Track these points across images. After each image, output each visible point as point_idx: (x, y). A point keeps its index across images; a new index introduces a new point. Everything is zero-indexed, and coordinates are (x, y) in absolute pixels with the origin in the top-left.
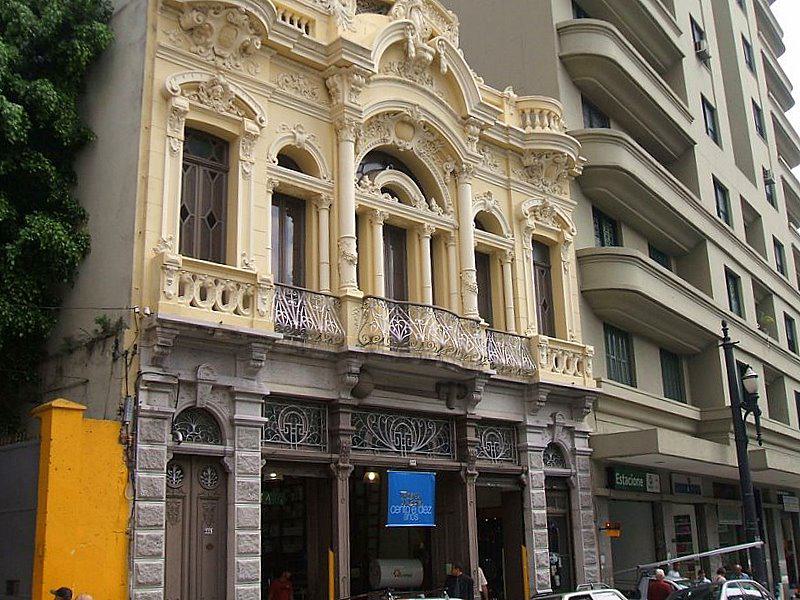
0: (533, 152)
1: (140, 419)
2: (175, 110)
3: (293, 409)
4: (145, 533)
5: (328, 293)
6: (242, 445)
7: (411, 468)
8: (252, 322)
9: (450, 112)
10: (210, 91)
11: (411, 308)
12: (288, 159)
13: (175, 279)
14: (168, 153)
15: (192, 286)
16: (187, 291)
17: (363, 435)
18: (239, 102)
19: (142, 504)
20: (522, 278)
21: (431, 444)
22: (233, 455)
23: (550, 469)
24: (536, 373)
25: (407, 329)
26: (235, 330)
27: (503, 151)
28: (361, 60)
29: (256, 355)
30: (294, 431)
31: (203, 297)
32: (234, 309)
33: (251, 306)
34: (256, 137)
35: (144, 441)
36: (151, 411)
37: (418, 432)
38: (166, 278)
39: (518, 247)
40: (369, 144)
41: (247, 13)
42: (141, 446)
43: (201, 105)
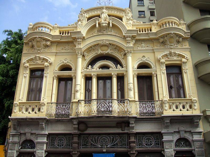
2: (25, 67)
3: (60, 137)
6: (38, 149)
7: (104, 152)
8: (192, 112)
9: (119, 37)
12: (143, 66)
14: (162, 74)
15: (187, 106)
17: (87, 143)
20: (160, 80)
21: (117, 144)
23: (178, 149)
27: (151, 41)
28: (132, 33)
29: (40, 123)
34: (186, 62)
35: (10, 149)
40: (89, 57)
41: (39, 37)
42: (9, 151)
43: (169, 59)
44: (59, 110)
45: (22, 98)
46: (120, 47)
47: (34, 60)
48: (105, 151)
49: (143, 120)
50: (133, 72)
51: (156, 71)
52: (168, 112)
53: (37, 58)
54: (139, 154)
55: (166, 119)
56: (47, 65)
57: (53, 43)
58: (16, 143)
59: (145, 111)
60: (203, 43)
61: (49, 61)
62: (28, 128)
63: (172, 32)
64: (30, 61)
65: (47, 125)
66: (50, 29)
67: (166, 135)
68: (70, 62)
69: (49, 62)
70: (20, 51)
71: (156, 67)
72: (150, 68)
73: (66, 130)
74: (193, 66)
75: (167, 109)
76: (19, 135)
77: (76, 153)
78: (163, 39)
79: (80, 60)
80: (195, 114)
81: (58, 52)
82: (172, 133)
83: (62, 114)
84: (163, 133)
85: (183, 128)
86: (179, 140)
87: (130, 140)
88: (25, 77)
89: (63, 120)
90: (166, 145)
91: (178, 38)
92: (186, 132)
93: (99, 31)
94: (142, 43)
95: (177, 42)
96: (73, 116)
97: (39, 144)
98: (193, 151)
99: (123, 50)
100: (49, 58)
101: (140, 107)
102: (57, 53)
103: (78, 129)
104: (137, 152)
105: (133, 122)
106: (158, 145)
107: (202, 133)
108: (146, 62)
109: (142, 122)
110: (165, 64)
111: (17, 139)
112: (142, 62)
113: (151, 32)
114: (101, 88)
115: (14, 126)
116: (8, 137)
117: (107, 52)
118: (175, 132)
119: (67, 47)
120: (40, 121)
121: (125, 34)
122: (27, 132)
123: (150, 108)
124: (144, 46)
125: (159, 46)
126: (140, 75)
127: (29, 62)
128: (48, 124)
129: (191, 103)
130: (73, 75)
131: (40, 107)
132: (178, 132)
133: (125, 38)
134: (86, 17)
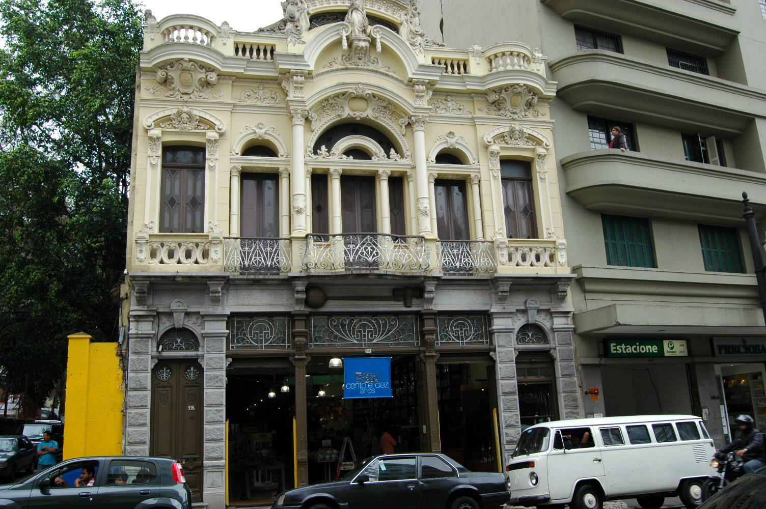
0: (494, 90)
1: (130, 340)
2: (492, 153)
4: (133, 411)
5: (483, 240)
7: (368, 355)
9: (397, 79)
10: (179, 119)
11: (379, 237)
13: (505, 253)
15: (516, 255)
16: (513, 257)
18: (531, 138)
19: (131, 393)
22: (203, 357)
23: (523, 347)
24: (496, 271)
25: (377, 253)
26: (189, 275)
30: (462, 334)
31: (524, 259)
32: (530, 263)
33: (555, 261)
34: (545, 155)
36: (137, 334)
37: (379, 328)
38: (500, 252)
39: (484, 170)
40: (321, 125)
41: (190, 60)
42: (131, 357)
44: (256, 255)
45: (152, 222)
46: (396, 106)
47: (174, 122)
48: (370, 352)
49: (452, 283)
50: (428, 170)
51: (479, 172)
52: (506, 269)
53: (185, 116)
54: (443, 358)
55: (502, 282)
56: (212, 139)
57: (222, 77)
58: (149, 338)
59: (269, 264)
60: (579, 111)
61: (220, 127)
62: (178, 300)
63: (522, 82)
64: (162, 122)
65: (225, 292)
66: (211, 35)
67: (499, 317)
68: (271, 133)
69: (220, 129)
70: (129, 92)
71: (479, 162)
72: (462, 164)
73: (275, 303)
74: (557, 165)
75: (504, 261)
76: (154, 317)
77: (304, 357)
78: (497, 96)
79: (299, 130)
80: (562, 275)
81: (237, 102)
82: (511, 313)
83: (244, 265)
84: (553, 312)
85: (538, 301)
86: (525, 328)
87: (294, 331)
88: (153, 165)
89: (269, 280)
90: (498, 340)
91: (531, 97)
92: (539, 311)
93: (348, 57)
94: (446, 100)
95: (526, 105)
96: (295, 272)
97: (210, 338)
98: (552, 352)
99: (403, 115)
100: (217, 119)
101: (467, 255)
102: (235, 105)
103: (307, 303)
104: (438, 355)
105: (433, 288)
106: (283, 341)
107: (571, 315)
108: (457, 147)
109: (450, 287)
110: (498, 158)
111: (150, 327)
112: (446, 147)
113: (466, 75)
114: (269, 201)
115: (142, 295)
116: (123, 320)
117: (364, 115)
118: (518, 311)
119: (261, 92)
120: (212, 282)
121: (414, 74)
122: (176, 311)
123: (467, 257)
124: (451, 108)
125: (486, 110)
126: (348, 173)
127: (161, 124)
128: (227, 290)
129: (553, 250)
130: (282, 168)
131: (207, 247)
132: (524, 312)
133: (411, 83)
134: (308, 13)
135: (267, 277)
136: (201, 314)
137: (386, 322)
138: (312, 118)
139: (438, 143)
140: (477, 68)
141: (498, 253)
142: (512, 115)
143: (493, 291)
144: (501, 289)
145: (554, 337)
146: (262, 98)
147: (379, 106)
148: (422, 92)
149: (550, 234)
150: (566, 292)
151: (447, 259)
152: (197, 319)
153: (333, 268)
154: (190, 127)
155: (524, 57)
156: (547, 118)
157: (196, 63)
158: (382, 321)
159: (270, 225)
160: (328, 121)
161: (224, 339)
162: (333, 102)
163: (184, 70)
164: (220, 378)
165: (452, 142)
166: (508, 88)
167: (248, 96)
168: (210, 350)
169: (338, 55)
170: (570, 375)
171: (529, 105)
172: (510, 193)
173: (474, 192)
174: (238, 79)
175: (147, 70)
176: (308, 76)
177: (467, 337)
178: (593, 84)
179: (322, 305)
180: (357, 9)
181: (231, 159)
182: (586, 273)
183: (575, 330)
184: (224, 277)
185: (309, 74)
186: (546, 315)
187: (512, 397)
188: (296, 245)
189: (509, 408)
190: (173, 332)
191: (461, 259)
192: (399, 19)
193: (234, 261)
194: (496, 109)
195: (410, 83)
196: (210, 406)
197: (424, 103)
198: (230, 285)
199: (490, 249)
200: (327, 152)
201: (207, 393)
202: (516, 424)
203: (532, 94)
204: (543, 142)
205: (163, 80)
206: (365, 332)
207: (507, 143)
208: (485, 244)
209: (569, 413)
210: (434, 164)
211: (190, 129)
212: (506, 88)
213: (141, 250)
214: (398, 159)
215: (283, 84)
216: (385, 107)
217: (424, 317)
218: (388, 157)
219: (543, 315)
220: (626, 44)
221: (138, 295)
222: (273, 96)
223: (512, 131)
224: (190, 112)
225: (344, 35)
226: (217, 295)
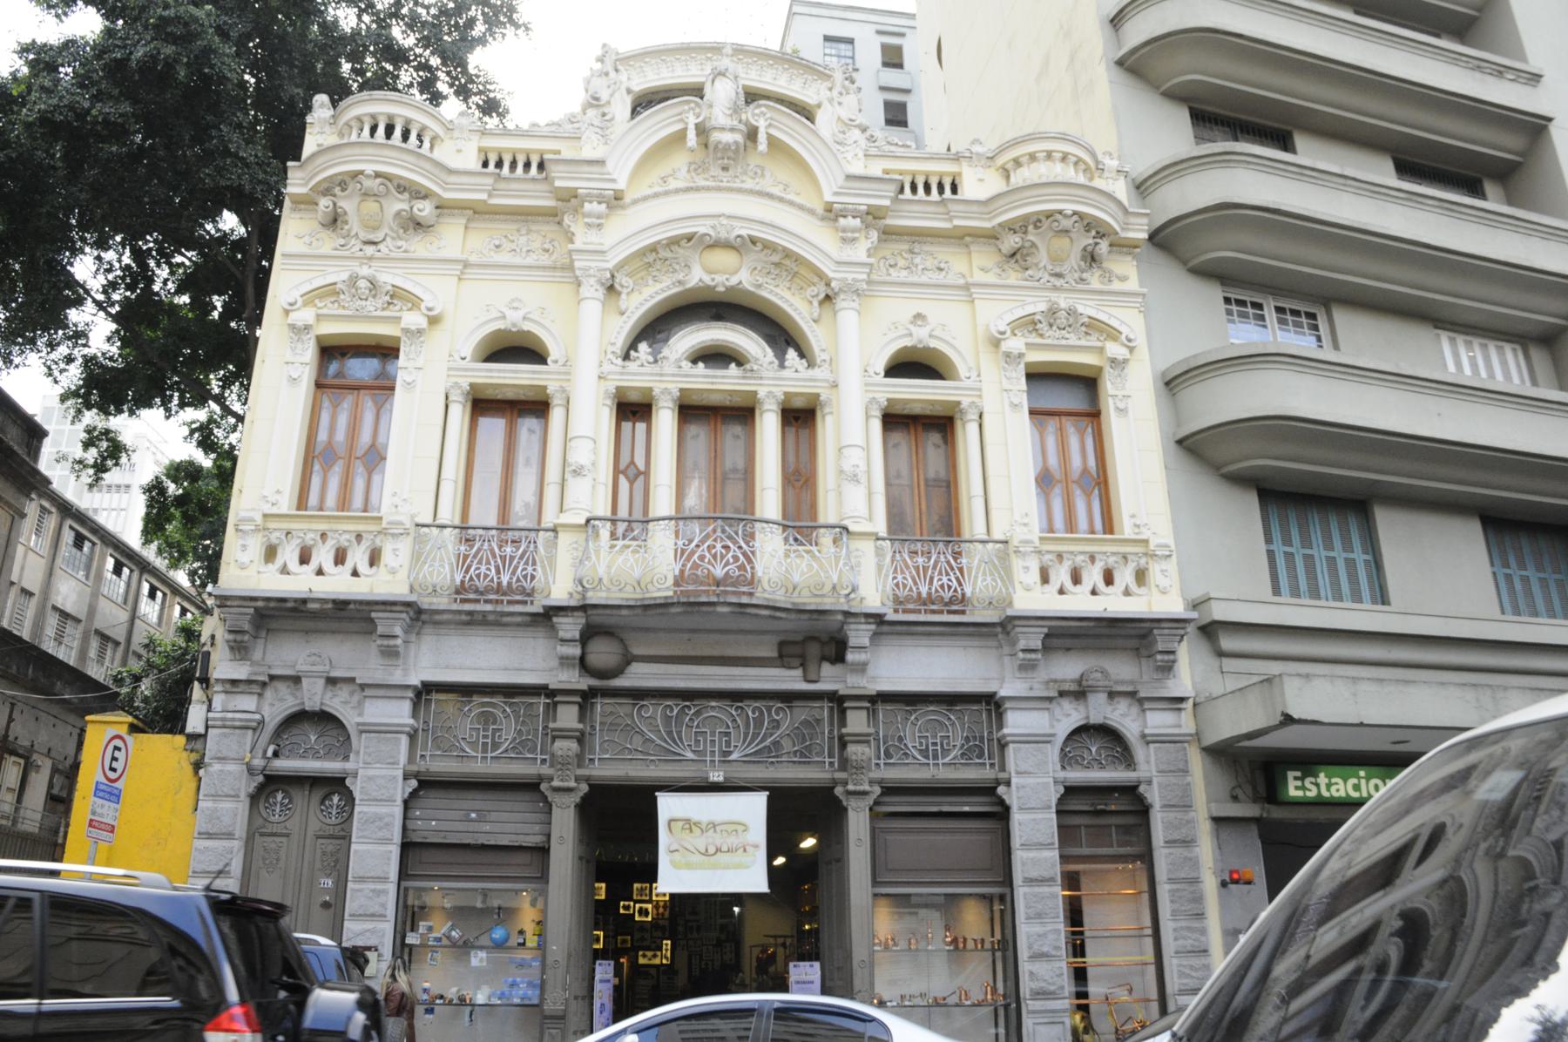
2: (1008, 355)
5: (985, 537)
9: (801, 207)
13: (1034, 565)
22: (355, 775)
23: (1078, 776)
24: (1010, 604)
31: (1076, 579)
32: (1090, 588)
34: (1125, 361)
40: (643, 299)
41: (378, 175)
45: (278, 492)
47: (342, 296)
51: (980, 396)
52: (1033, 599)
53: (363, 284)
58: (247, 728)
71: (979, 375)
77: (572, 784)
79: (592, 307)
86: (1082, 731)
90: (1015, 757)
91: (1091, 241)
98: (1142, 789)
99: (816, 280)
107: (1189, 705)
108: (932, 346)
110: (1022, 366)
115: (239, 637)
117: (734, 281)
119: (523, 239)
121: (836, 194)
122: (309, 674)
125: (998, 271)
127: (317, 301)
129: (1143, 561)
131: (378, 542)
133: (831, 214)
134: (629, 91)
135: (499, 608)
136: (358, 681)
137: (762, 713)
138: (622, 286)
139: (892, 335)
140: (978, 184)
141: (1017, 564)
142: (1053, 279)
143: (1006, 650)
144: (1022, 644)
145: (1148, 756)
146: (524, 249)
147: (766, 262)
148: (853, 231)
149: (1138, 526)
150: (1173, 652)
151: (900, 577)
152: (352, 693)
153: (638, 589)
154: (370, 306)
155: (1076, 164)
156: (1133, 284)
157: (390, 180)
158: (754, 713)
159: (527, 505)
160: (657, 293)
161: (404, 740)
162: (667, 254)
163: (366, 195)
164: (386, 820)
165: (920, 337)
166: (1040, 221)
167: (497, 247)
168: (369, 760)
169: (679, 162)
170: (1184, 842)
171: (1091, 258)
172: (1051, 442)
173: (967, 435)
174: (478, 212)
175: (299, 201)
176: (616, 202)
177: (946, 752)
178: (1226, 214)
179: (618, 672)
180: (724, 75)
181: (449, 369)
182: (1220, 612)
183: (1197, 736)
184: (408, 604)
185: (616, 199)
186: (1130, 705)
187: (1045, 890)
188: (565, 539)
189: (1039, 916)
190: (298, 718)
191: (932, 579)
192: (815, 97)
193: (431, 574)
194: (1018, 268)
195: (828, 214)
196: (361, 879)
197: (859, 252)
198: (424, 623)
199: (999, 558)
200: (650, 354)
201: (356, 851)
202: (1054, 953)
203: (1093, 233)
204: (1121, 333)
205: (330, 218)
206: (713, 733)
207: (1041, 336)
208: (990, 546)
209: (1182, 928)
210: (880, 378)
211: (372, 309)
212: (1037, 221)
213: (244, 546)
214: (800, 368)
215: (567, 220)
216: (777, 265)
217: (846, 705)
218: (782, 366)
219: (1123, 705)
220: (1300, 141)
221: (231, 637)
222: (546, 246)
223: (1053, 312)
224: (374, 276)
225: (692, 121)
226: (392, 642)
